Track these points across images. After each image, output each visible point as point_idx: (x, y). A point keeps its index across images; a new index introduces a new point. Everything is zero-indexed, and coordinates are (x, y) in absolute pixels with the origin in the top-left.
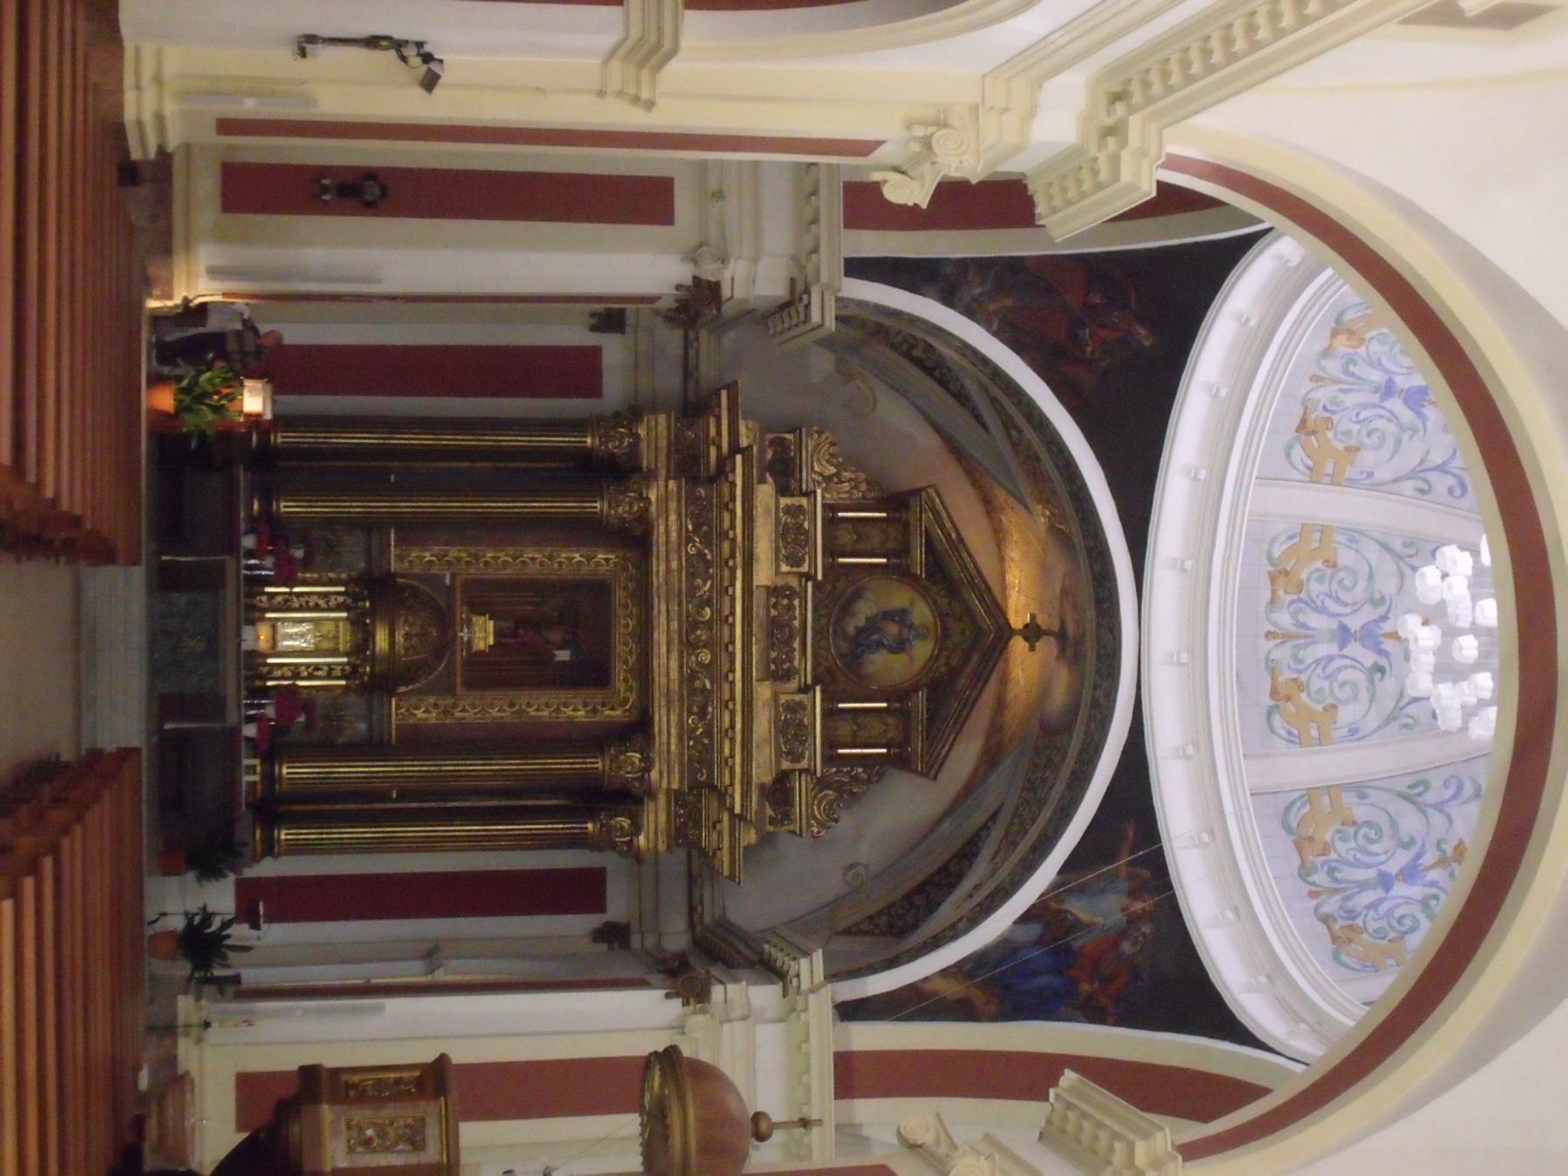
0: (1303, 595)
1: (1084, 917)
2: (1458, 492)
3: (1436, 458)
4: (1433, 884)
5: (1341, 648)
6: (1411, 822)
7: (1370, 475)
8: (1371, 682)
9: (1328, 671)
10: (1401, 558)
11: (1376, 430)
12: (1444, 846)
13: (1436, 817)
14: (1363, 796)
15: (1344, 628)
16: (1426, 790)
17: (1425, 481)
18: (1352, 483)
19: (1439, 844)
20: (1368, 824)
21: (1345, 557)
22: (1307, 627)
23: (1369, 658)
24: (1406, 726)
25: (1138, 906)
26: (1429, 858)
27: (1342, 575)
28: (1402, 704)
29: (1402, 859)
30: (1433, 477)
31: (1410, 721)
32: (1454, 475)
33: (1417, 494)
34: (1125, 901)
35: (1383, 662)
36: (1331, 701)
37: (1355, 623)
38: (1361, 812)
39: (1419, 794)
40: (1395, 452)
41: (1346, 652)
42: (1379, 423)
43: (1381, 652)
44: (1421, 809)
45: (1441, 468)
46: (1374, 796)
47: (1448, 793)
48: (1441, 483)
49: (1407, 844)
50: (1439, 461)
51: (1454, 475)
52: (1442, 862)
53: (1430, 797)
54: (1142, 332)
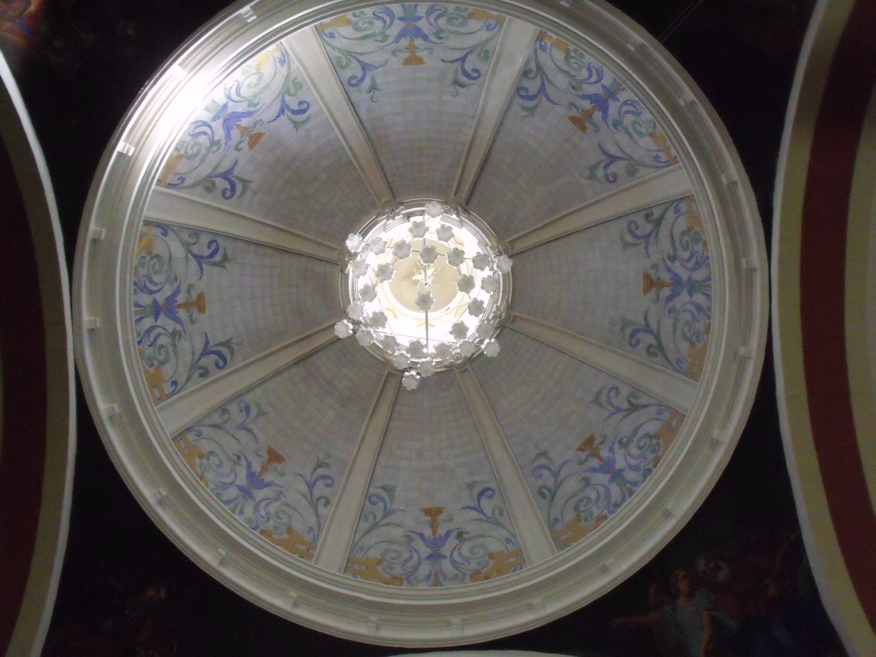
0: (404, 577)
1: (706, 634)
2: (228, 194)
3: (304, 488)
4: (611, 450)
5: (445, 557)
6: (571, 485)
7: (311, 529)
8: (470, 539)
9: (463, 562)
10: (376, 524)
11: (276, 513)
12: (583, 458)
13: (564, 473)
14: (556, 520)
15: (430, 557)
16: (546, 488)
17: (320, 498)
18: (315, 539)
19: (581, 463)
20: (576, 509)
21: (374, 554)
22: (430, 575)
23: (452, 542)
24: (501, 513)
25: (683, 586)
26: (594, 463)
27: (388, 557)
28: (485, 518)
29: (601, 478)
30: (317, 493)
31: (497, 512)
32: (214, 352)
33: (329, 506)
34: (682, 602)
35: (455, 534)
36: (487, 557)
37: (425, 551)
38: (569, 516)
39: (549, 490)
40: (295, 509)
41: (448, 554)
42: (272, 508)
43: (447, 535)
44: (558, 485)
45: (311, 486)
46: (555, 514)
47: (545, 472)
48: (320, 489)
49: (586, 481)
50: (306, 487)
51: (316, 480)
52: (595, 454)
53: (550, 482)
54: (150, 593)
